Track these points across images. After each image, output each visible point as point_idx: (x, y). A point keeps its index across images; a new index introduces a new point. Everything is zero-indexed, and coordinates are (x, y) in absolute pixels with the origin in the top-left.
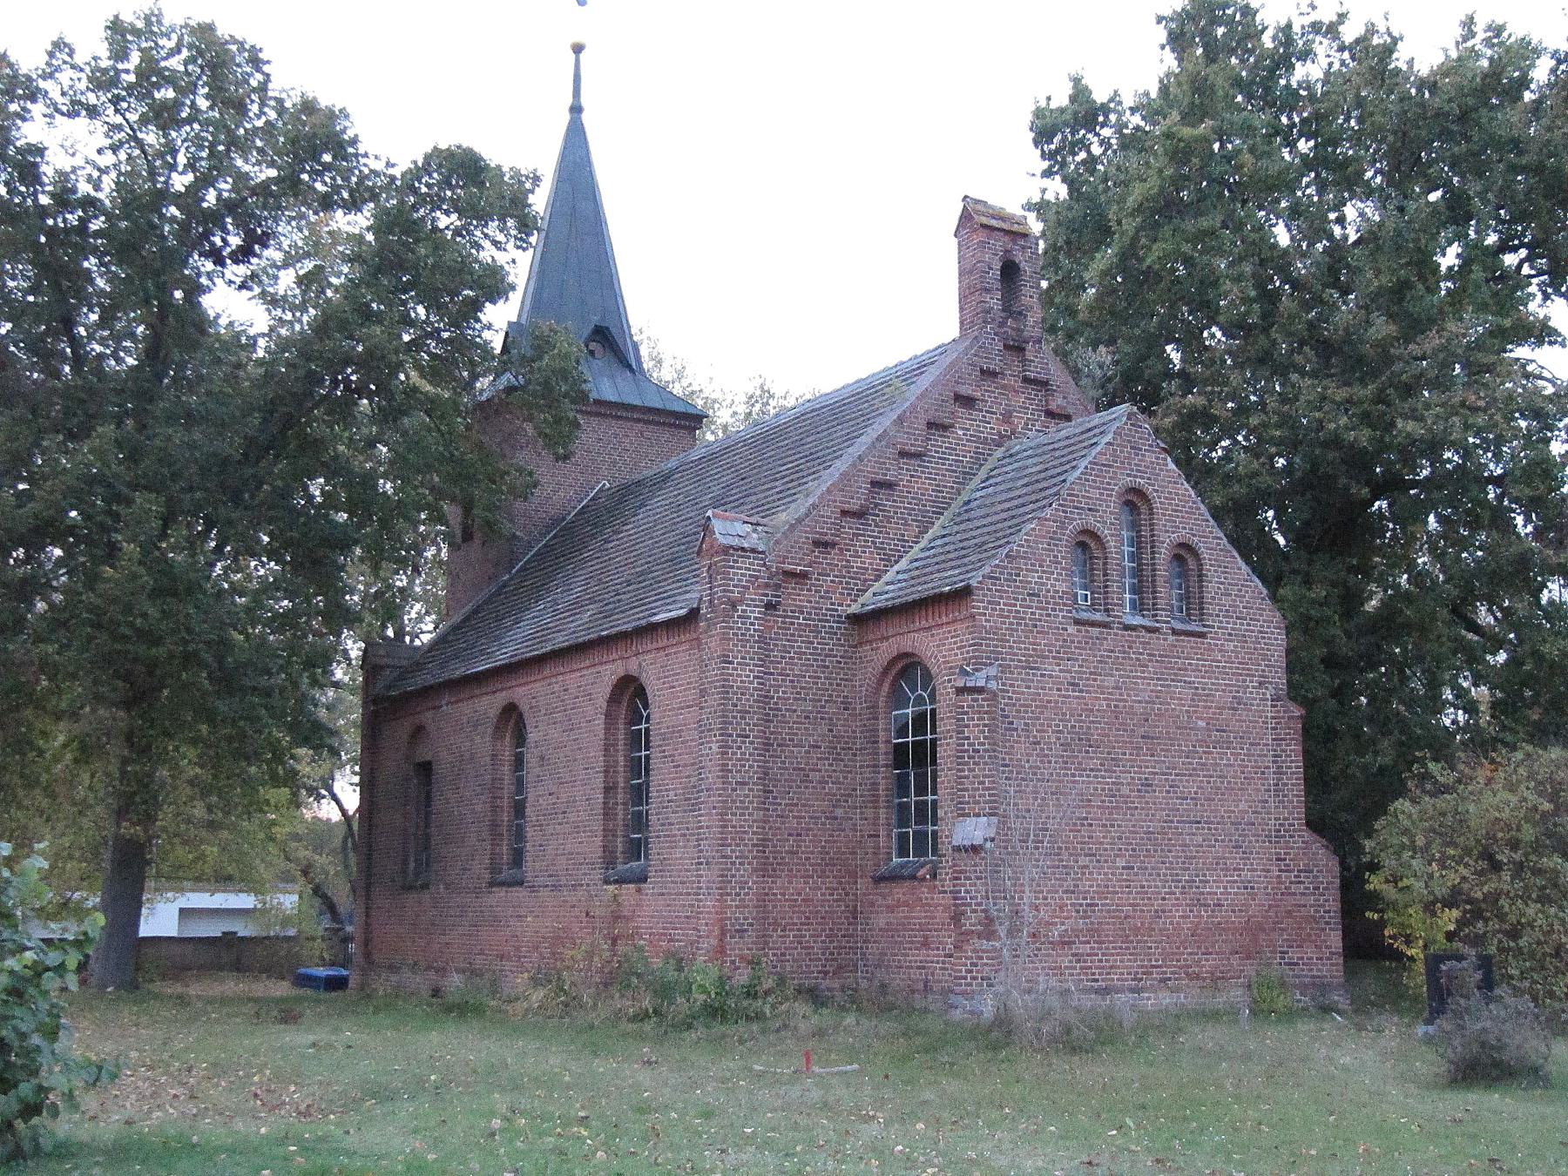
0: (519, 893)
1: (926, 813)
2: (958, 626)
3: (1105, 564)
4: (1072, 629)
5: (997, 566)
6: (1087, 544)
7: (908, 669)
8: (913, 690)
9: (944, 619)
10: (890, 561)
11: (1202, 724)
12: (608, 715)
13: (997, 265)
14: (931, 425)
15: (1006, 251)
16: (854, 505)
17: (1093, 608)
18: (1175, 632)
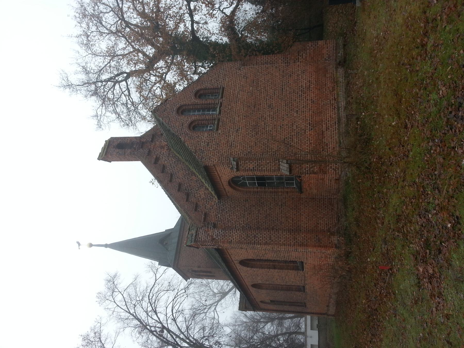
0: (307, 287)
1: (280, 178)
2: (218, 169)
3: (200, 120)
4: (220, 132)
5: (198, 157)
6: (194, 126)
7: (234, 182)
8: (241, 181)
9: (216, 173)
10: (203, 186)
11: (251, 88)
12: (252, 267)
13: (118, 150)
14: (163, 172)
15: (114, 147)
16: (185, 197)
17: (214, 124)
18: (222, 97)
